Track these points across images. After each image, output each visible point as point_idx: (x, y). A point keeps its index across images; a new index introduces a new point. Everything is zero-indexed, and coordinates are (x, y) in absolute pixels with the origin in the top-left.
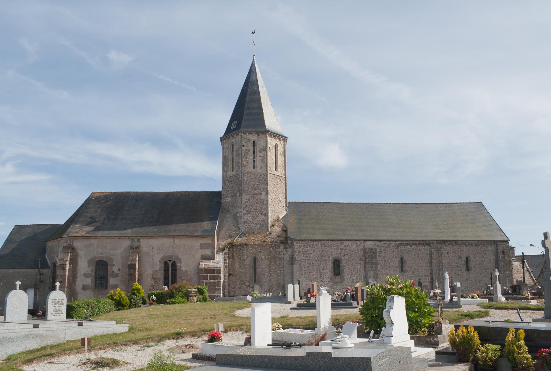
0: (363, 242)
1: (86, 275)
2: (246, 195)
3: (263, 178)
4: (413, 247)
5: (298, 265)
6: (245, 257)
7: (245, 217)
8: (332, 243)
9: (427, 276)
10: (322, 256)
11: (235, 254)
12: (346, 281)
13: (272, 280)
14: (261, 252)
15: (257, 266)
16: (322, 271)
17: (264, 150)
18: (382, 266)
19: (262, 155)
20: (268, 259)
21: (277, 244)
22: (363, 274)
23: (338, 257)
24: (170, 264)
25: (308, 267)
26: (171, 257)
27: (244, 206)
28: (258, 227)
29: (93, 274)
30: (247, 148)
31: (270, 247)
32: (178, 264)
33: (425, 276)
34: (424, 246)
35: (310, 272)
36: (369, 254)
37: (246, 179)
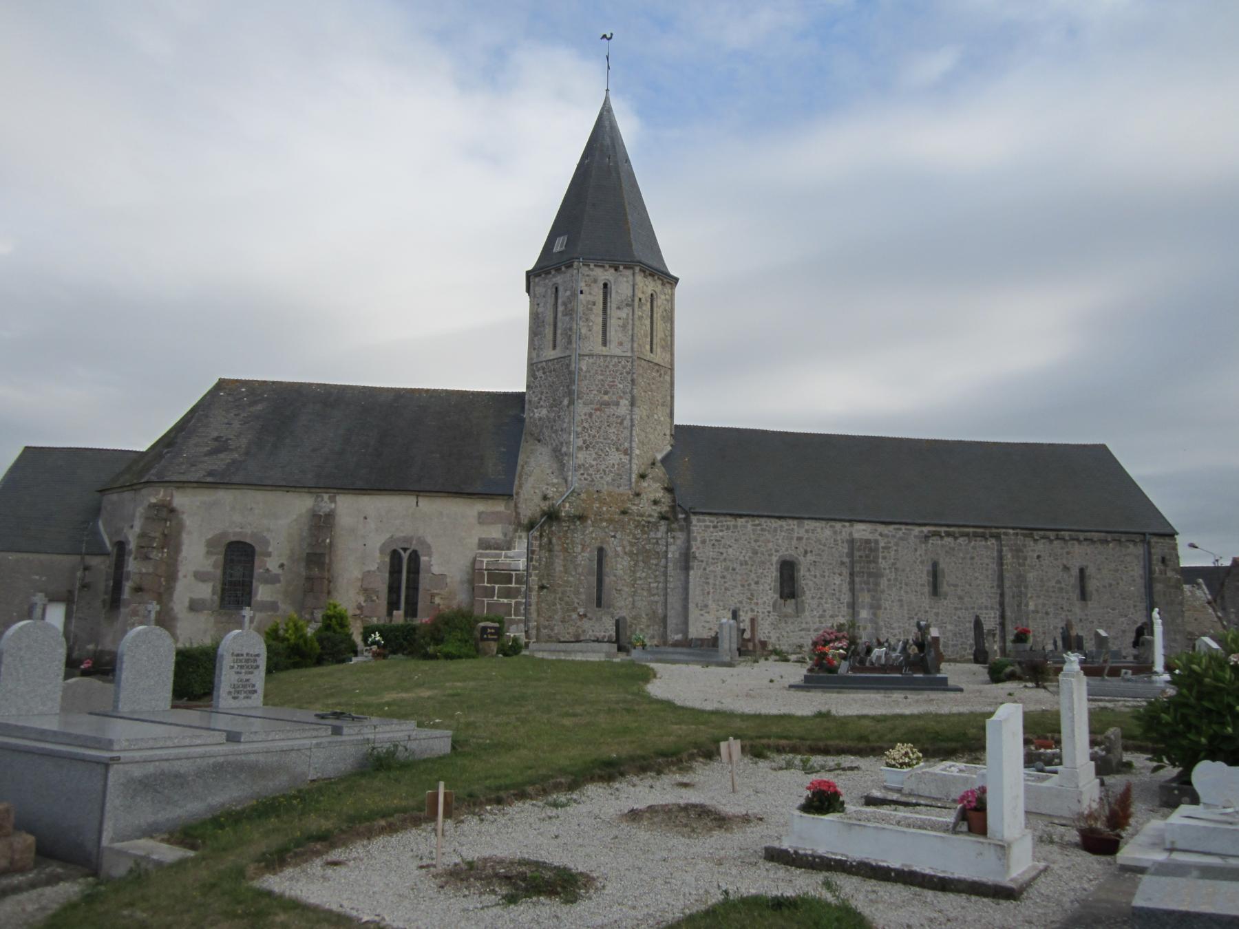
4: (961, 540)
5: (700, 572)
8: (780, 522)
9: (992, 608)
10: (755, 553)
11: (554, 540)
12: (807, 613)
13: (639, 604)
14: (614, 537)
15: (607, 569)
16: (753, 586)
17: (627, 305)
18: (889, 580)
19: (624, 316)
20: (631, 554)
22: (846, 598)
24: (405, 556)
26: (408, 539)
28: (609, 479)
29: (219, 572)
30: (591, 298)
31: (636, 527)
32: (423, 559)
34: (986, 539)
35: (726, 589)
36: (861, 553)
37: (584, 369)
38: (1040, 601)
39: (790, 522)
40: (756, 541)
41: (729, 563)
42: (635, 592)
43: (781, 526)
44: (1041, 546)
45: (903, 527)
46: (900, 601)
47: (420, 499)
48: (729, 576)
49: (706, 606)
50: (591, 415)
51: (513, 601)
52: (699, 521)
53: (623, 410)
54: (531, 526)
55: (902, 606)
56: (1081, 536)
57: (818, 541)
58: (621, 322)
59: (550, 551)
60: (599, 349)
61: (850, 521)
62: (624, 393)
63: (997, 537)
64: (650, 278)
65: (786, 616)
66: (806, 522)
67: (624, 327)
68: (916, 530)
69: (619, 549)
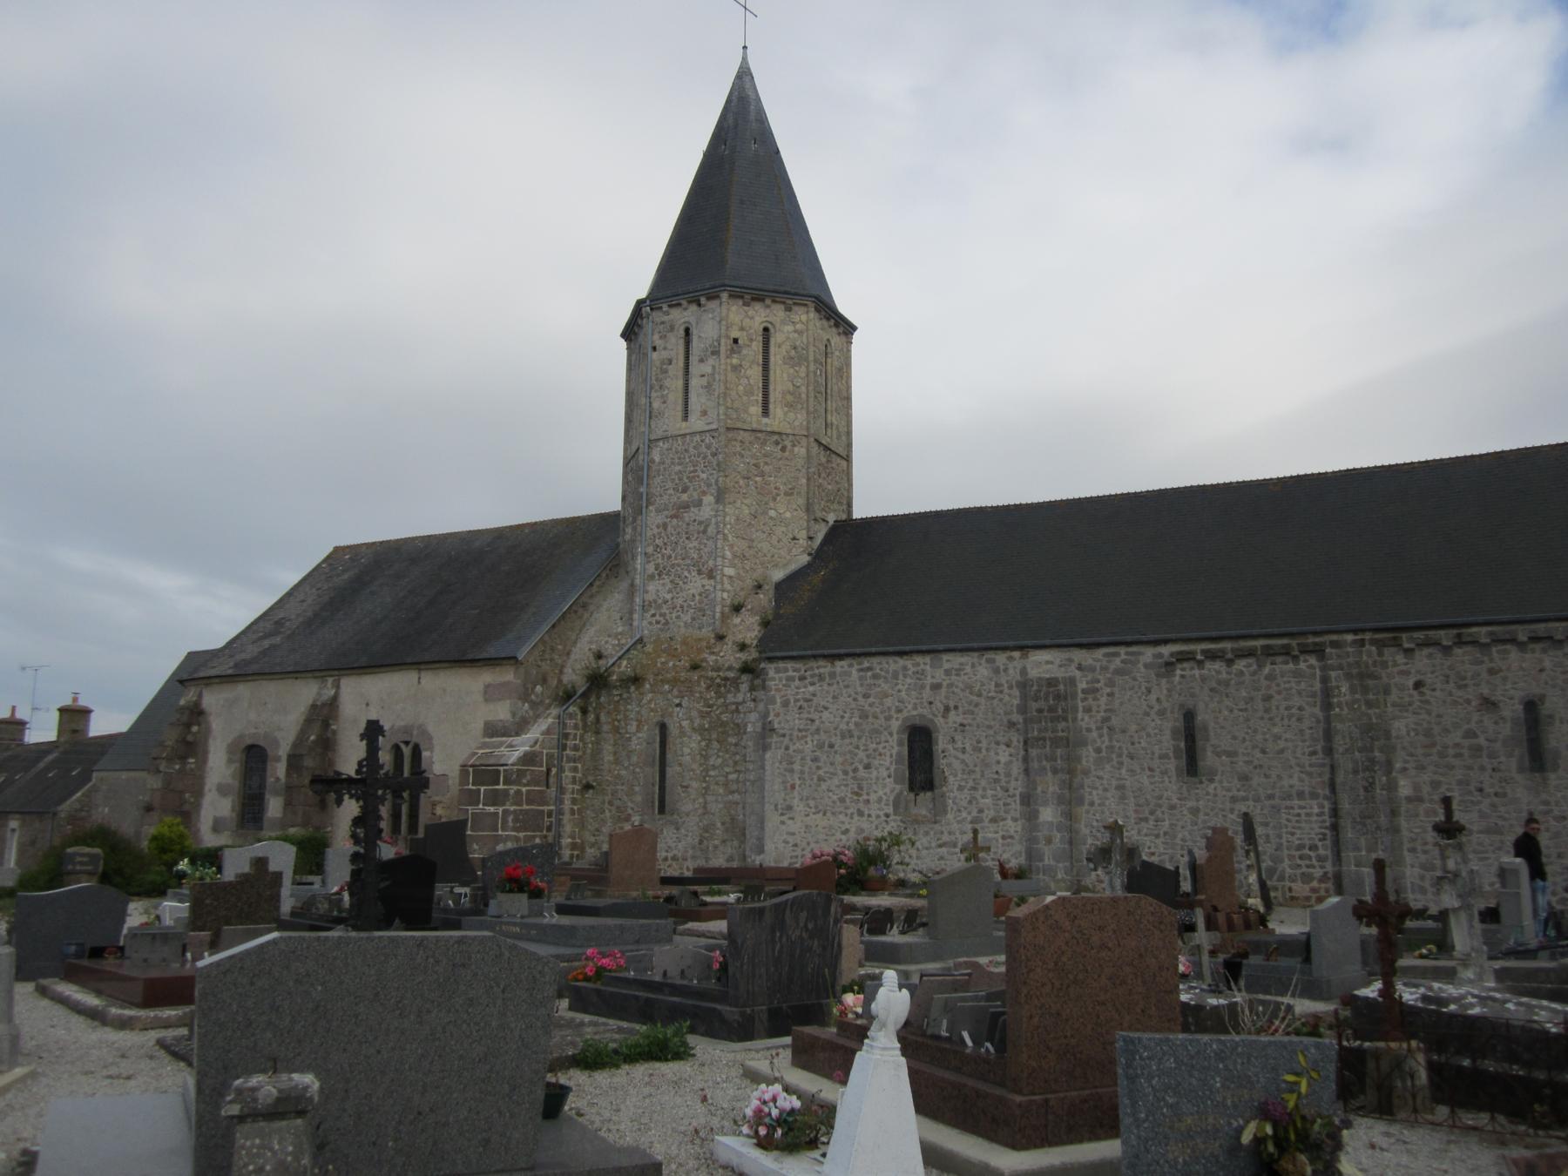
0: (1016, 654)
1: (222, 790)
2: (658, 511)
3: (708, 447)
4: (1241, 664)
5: (780, 752)
6: (633, 727)
7: (651, 587)
8: (901, 662)
9: (1314, 796)
10: (864, 716)
11: (603, 718)
12: (950, 816)
13: (713, 807)
14: (679, 705)
15: (669, 756)
16: (862, 773)
17: (713, 353)
18: (1098, 751)
19: (709, 370)
20: (700, 730)
21: (731, 675)
22: (1017, 787)
23: (921, 716)
24: (407, 751)
25: (815, 760)
26: (407, 730)
27: (650, 550)
28: (687, 618)
29: (236, 784)
30: (665, 354)
31: (708, 688)
32: (425, 754)
33: (1301, 795)
34: (1295, 659)
35: (820, 779)
36: (1041, 704)
37: (657, 459)
38: (1426, 777)
39: (919, 659)
40: (866, 696)
41: (823, 736)
42: (707, 789)
43: (905, 668)
44: (1423, 662)
45: (1122, 650)
46: (1120, 788)
47: (423, 674)
48: (824, 758)
49: (790, 808)
50: (665, 526)
51: (500, 810)
52: (778, 671)
53: (706, 512)
54: (567, 696)
55: (1123, 797)
56: (1522, 633)
57: (969, 687)
58: (704, 381)
59: (597, 732)
60: (678, 426)
61: (1021, 648)
62: (709, 485)
63: (1318, 651)
64: (758, 306)
65: (916, 821)
66: (945, 657)
67: (708, 387)
68: (1148, 653)
69: (685, 723)
